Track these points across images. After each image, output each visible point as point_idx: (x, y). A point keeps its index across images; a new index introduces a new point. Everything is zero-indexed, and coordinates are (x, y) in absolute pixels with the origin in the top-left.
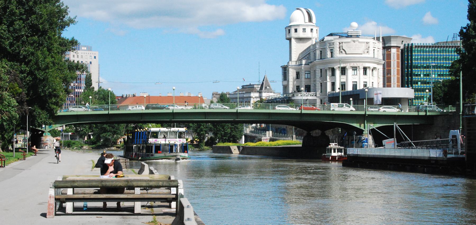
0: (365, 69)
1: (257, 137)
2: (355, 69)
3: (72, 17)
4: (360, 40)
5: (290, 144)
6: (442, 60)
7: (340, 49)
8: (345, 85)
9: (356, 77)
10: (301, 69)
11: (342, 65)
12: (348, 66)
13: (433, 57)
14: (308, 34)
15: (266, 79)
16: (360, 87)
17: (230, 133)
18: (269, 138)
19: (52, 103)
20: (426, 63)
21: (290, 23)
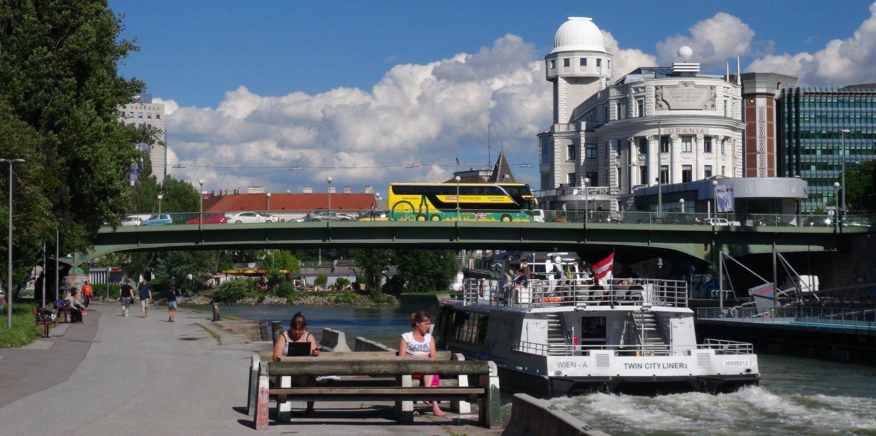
0: (708, 139)
2: (687, 138)
3: (129, 40)
4: (698, 81)
6: (858, 121)
7: (657, 100)
9: (689, 155)
11: (663, 131)
13: (841, 116)
14: (592, 69)
15: (504, 160)
20: (827, 128)
21: (555, 46)
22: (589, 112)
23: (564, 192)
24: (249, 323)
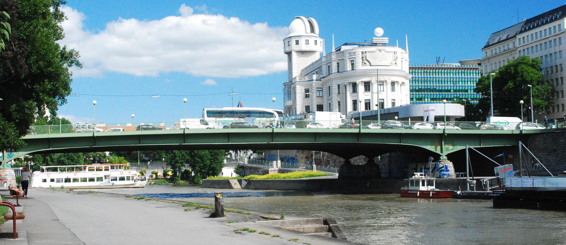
0: (393, 84)
1: (261, 168)
4: (388, 49)
5: (313, 176)
7: (363, 60)
8: (369, 103)
10: (311, 85)
11: (366, 79)
12: (373, 80)
14: (311, 47)
16: (388, 105)
17: (209, 166)
18: (277, 169)
19: (44, 92)
24: (307, 222)
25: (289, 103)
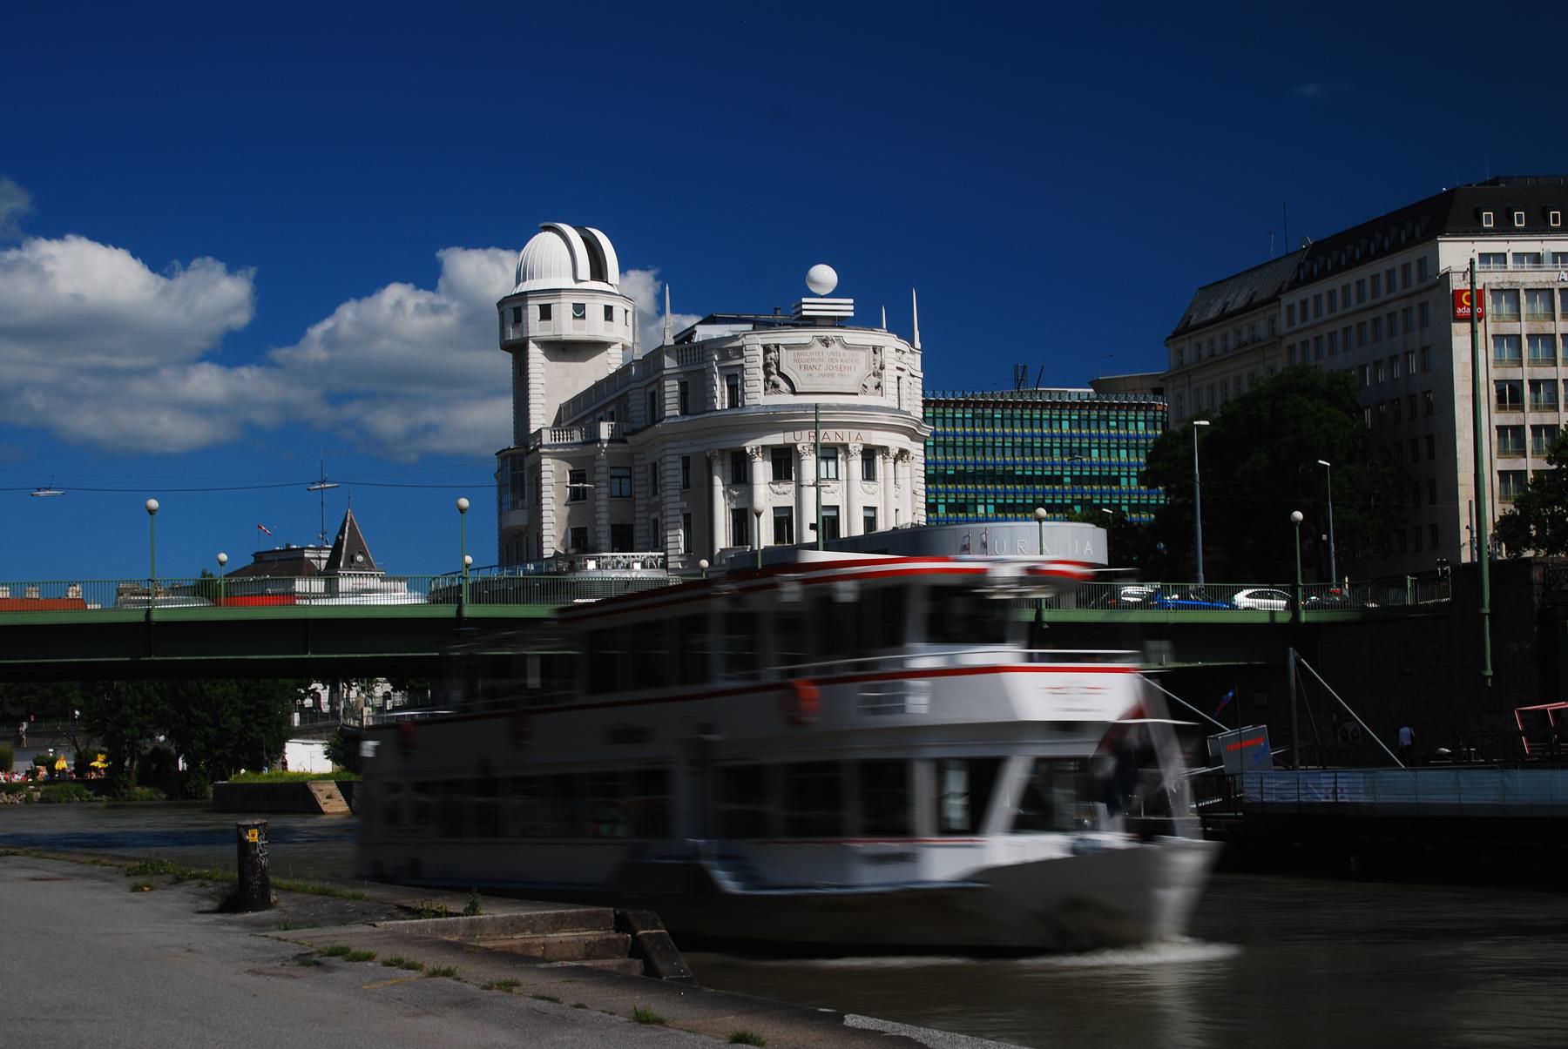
0: (869, 454)
4: (852, 336)
7: (768, 374)
11: (777, 439)
12: (803, 440)
14: (594, 327)
15: (352, 527)
21: (518, 283)
22: (607, 404)
23: (572, 563)
25: (518, 519)
